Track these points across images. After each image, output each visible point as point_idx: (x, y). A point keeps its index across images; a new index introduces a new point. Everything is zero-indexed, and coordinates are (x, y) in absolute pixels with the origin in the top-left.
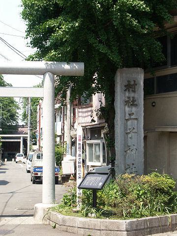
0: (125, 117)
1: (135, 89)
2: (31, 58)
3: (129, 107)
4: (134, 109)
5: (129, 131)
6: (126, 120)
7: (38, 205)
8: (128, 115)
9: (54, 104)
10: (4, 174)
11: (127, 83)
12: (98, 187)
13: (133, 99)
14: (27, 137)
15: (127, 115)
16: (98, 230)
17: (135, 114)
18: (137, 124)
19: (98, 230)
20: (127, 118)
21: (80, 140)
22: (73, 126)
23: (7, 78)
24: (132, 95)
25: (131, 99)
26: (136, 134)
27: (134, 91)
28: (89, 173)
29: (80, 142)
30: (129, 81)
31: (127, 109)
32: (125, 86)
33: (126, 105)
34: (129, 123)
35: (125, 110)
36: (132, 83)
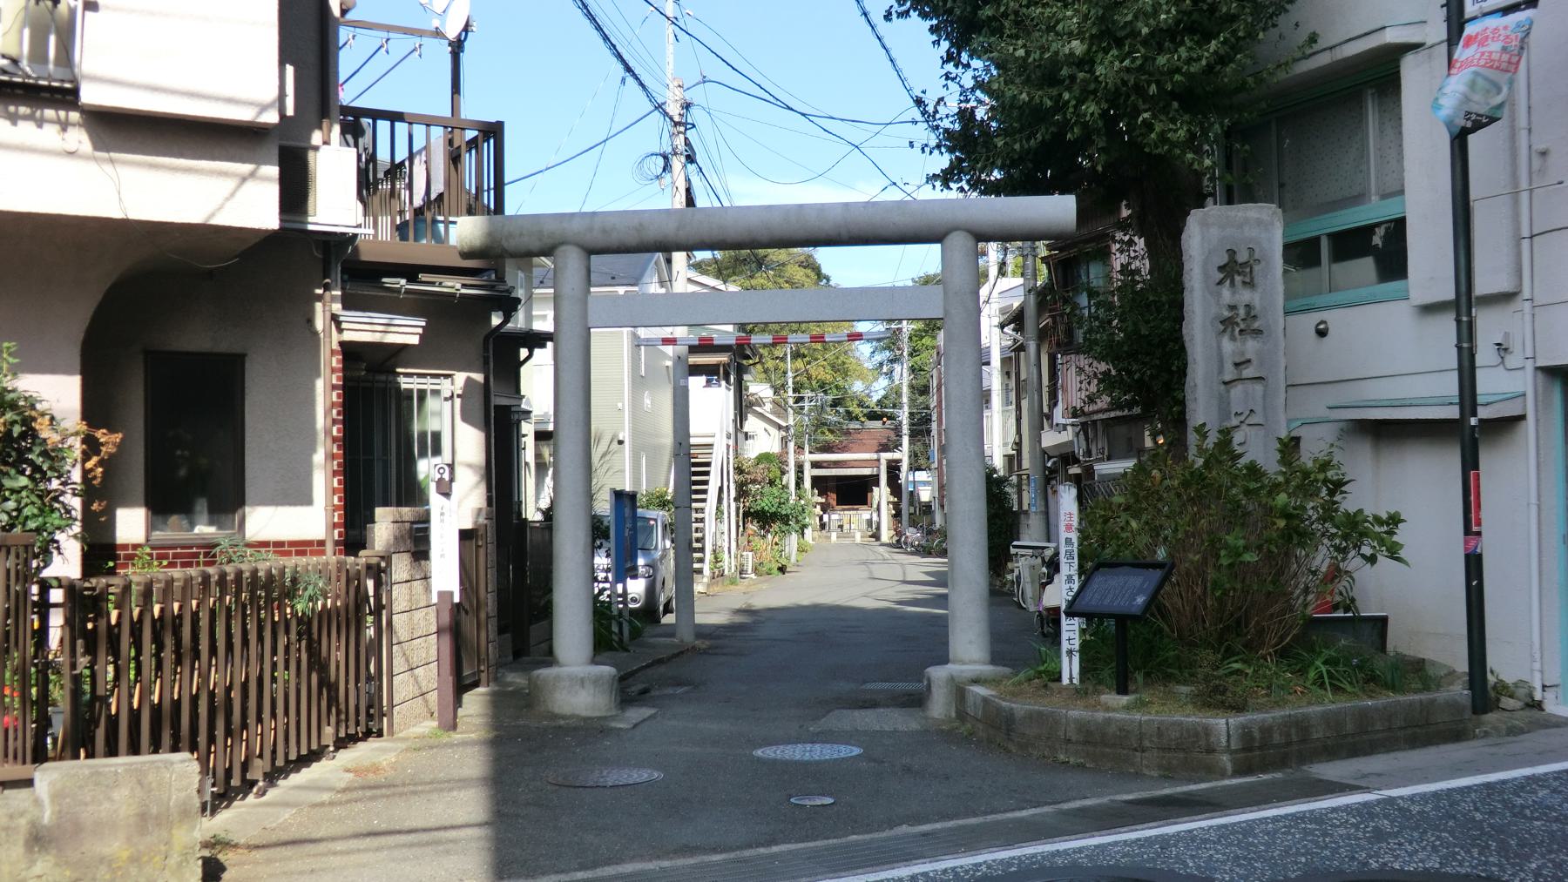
0: (1221, 371)
3: (1233, 338)
5: (1235, 422)
6: (1225, 383)
7: (938, 673)
10: (23, 793)
11: (1224, 259)
12: (1135, 610)
13: (1248, 313)
14: (899, 461)
15: (1229, 367)
16: (1466, 333)
17: (1255, 362)
18: (1264, 397)
19: (1466, 333)
20: (1227, 378)
21: (1069, 528)
22: (1050, 417)
23: (398, 160)
24: (1245, 296)
25: (1242, 312)
26: (1261, 432)
27: (1250, 284)
28: (1097, 567)
30: (1232, 253)
31: (1228, 346)
32: (1221, 269)
34: (1237, 391)
35: (1219, 347)
36: (1242, 257)
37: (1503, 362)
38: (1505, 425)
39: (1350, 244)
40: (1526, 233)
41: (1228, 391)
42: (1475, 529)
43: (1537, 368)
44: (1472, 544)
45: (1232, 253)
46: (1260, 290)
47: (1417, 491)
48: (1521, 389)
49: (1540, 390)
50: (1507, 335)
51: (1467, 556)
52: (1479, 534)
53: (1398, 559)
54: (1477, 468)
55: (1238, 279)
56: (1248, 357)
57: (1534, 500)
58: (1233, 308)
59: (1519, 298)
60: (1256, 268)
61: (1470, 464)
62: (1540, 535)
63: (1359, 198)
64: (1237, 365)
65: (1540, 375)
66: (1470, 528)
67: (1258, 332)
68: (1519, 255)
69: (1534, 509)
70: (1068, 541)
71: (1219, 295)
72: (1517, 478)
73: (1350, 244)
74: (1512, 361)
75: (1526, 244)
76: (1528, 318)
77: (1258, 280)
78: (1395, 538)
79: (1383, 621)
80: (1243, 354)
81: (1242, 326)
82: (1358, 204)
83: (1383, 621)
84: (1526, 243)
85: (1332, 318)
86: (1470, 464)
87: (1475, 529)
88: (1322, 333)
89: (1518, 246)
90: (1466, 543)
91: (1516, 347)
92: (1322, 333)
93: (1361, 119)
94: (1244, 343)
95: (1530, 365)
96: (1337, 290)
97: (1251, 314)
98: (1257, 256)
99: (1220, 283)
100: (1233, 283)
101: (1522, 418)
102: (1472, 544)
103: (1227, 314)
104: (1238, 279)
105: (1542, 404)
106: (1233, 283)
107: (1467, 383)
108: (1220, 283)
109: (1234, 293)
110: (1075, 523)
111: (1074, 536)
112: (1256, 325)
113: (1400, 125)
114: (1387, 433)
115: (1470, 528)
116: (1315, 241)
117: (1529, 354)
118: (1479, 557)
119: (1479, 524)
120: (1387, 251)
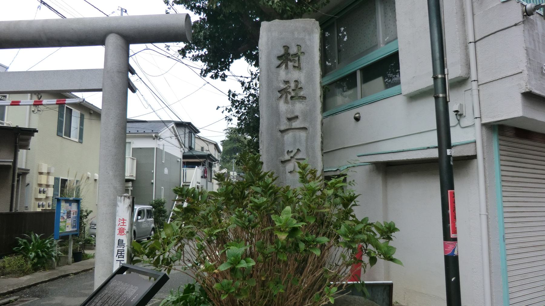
0: (278, 123)
1: (299, 64)
2: (472, 95)
3: (286, 102)
4: (299, 107)
5: (287, 157)
8: (286, 121)
9: (257, 53)
11: (282, 52)
13: (296, 86)
17: (286, 152)
20: (283, 128)
21: (121, 231)
24: (295, 75)
25: (293, 85)
27: (298, 68)
29: (121, 237)
30: (286, 48)
31: (283, 106)
32: (279, 58)
33: (281, 97)
36: (293, 50)
37: (459, 123)
38: (467, 160)
39: (371, 72)
40: (471, 39)
41: (283, 137)
42: (452, 236)
43: (484, 125)
44: (450, 248)
45: (286, 48)
46: (304, 71)
47: (414, 208)
48: (472, 139)
49: (485, 138)
50: (461, 106)
51: (447, 258)
52: (455, 240)
53: (392, 260)
54: (452, 188)
55: (290, 64)
56: (297, 114)
57: (484, 211)
58: (286, 82)
59: (470, 80)
60: (302, 57)
61: (447, 186)
62: (488, 235)
63: (375, 47)
64: (289, 119)
65: (484, 129)
66: (449, 234)
67: (304, 98)
68: (467, 55)
69: (484, 218)
70: (120, 242)
71: (278, 74)
72: (473, 196)
73: (371, 72)
74: (465, 122)
75: (471, 46)
76: (475, 92)
77: (303, 65)
78: (391, 243)
79: (390, 287)
80: (293, 112)
81: (293, 94)
82: (372, 51)
83: (390, 287)
84: (471, 46)
85: (363, 111)
86: (447, 186)
87: (452, 236)
88: (357, 119)
89: (466, 48)
90: (445, 247)
91: (467, 112)
92: (357, 119)
93: (373, 11)
94: (293, 105)
95: (478, 123)
96: (365, 96)
97: (298, 87)
98: (302, 50)
99: (279, 67)
100: (287, 66)
101: (475, 157)
102: (450, 248)
103: (283, 86)
104: (290, 64)
105: (486, 148)
106: (287, 66)
107: (443, 123)
108: (279, 67)
109: (287, 74)
110: (127, 227)
111: (125, 239)
112: (302, 93)
113: (395, 11)
114: (391, 170)
115: (449, 234)
116: (354, 74)
117: (477, 115)
118: (456, 259)
119: (455, 232)
120: (387, 68)
